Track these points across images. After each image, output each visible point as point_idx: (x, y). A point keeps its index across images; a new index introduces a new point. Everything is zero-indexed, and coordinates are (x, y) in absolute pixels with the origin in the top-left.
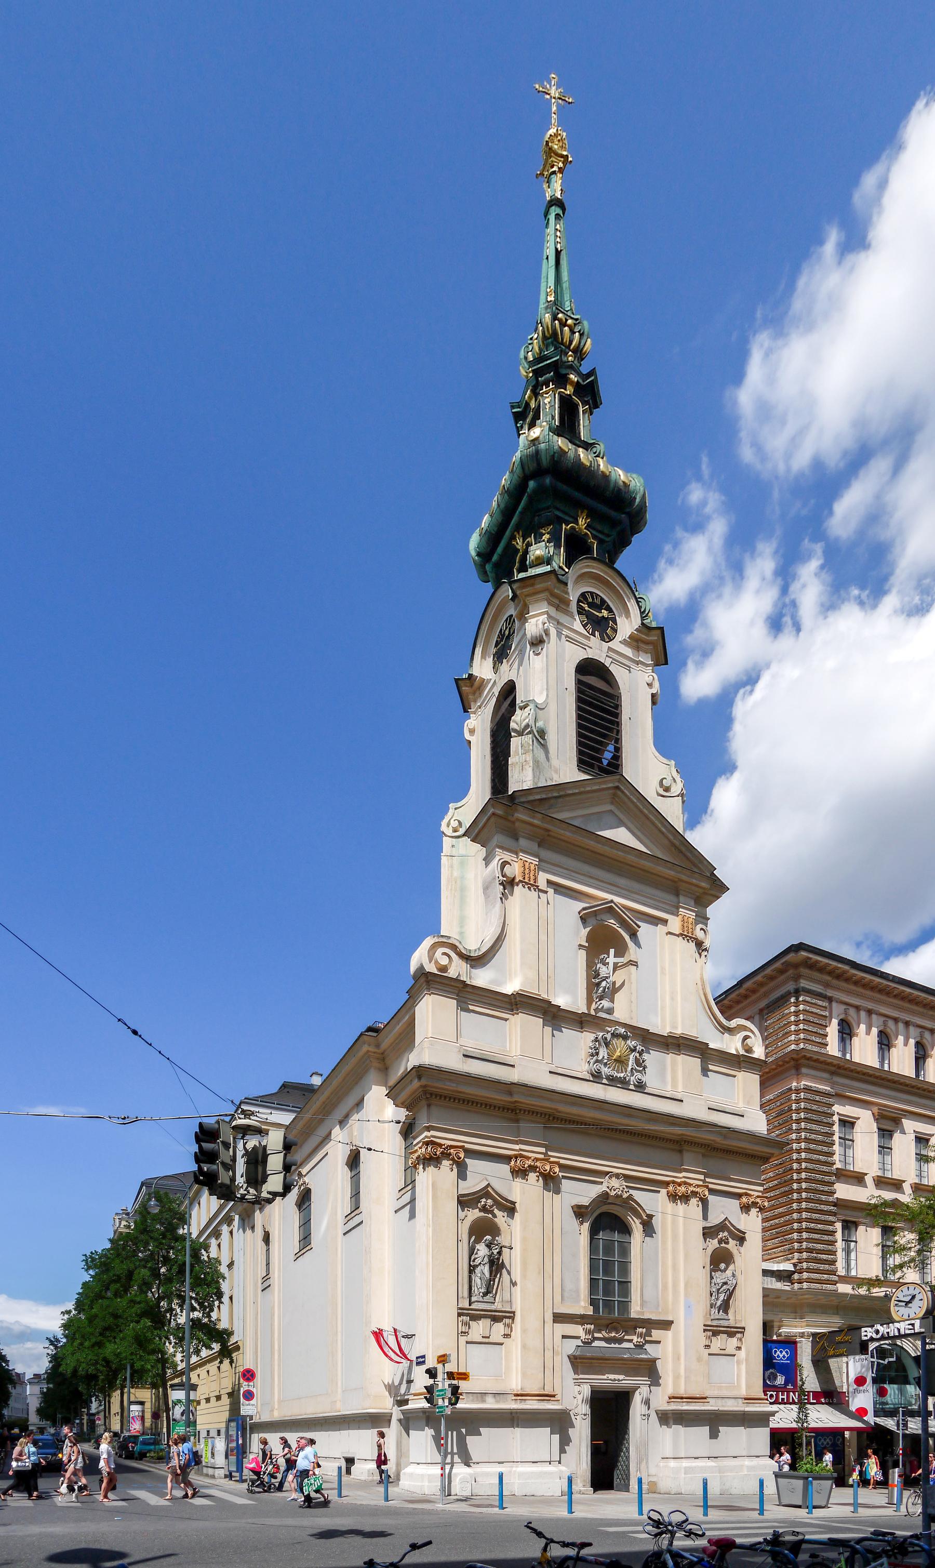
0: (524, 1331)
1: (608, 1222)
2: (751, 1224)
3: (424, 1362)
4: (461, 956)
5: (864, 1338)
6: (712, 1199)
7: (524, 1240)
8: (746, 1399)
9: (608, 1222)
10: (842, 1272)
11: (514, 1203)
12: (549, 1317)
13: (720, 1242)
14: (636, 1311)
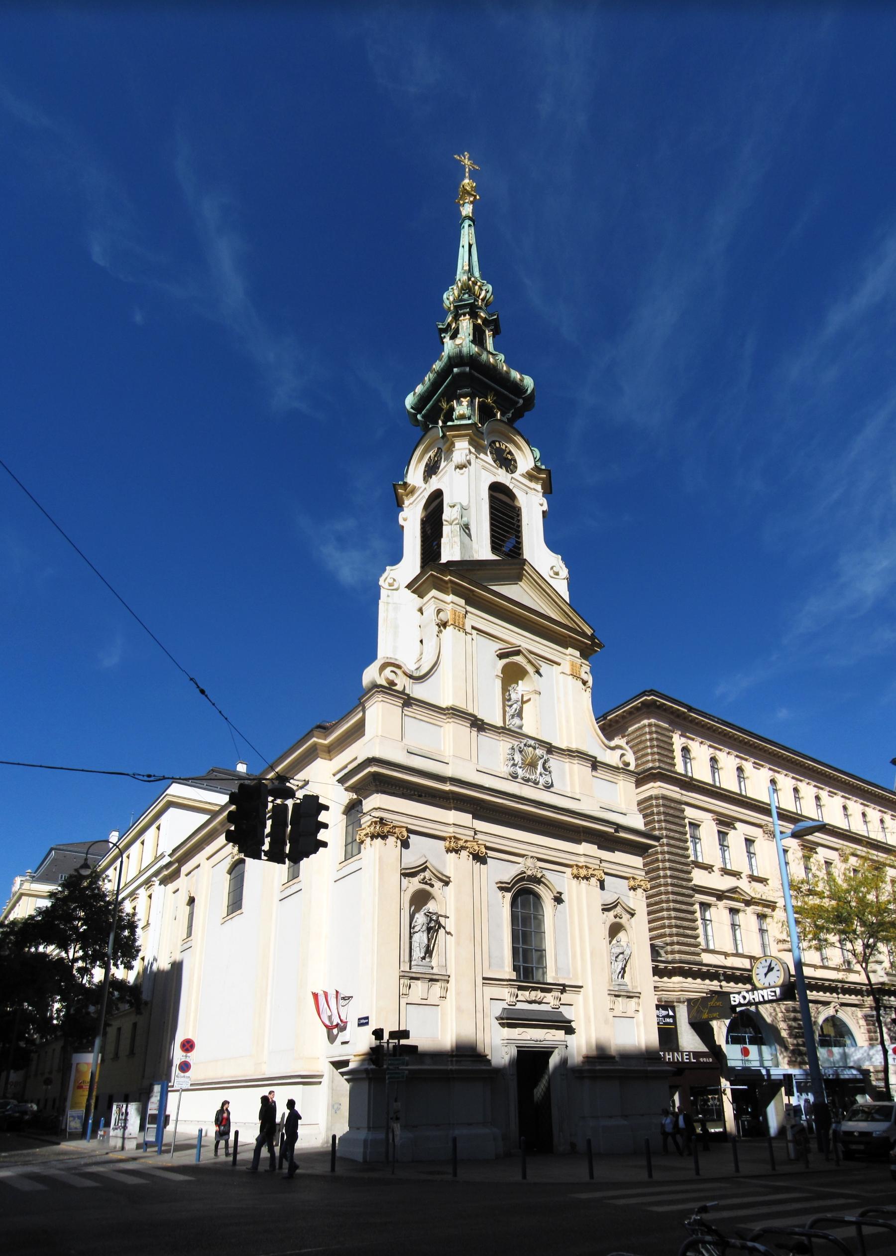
0: (458, 994)
1: (525, 897)
2: (638, 901)
4: (405, 673)
5: (733, 1003)
6: (608, 880)
8: (648, 1059)
9: (525, 897)
10: (703, 946)
12: (480, 981)
13: (615, 917)
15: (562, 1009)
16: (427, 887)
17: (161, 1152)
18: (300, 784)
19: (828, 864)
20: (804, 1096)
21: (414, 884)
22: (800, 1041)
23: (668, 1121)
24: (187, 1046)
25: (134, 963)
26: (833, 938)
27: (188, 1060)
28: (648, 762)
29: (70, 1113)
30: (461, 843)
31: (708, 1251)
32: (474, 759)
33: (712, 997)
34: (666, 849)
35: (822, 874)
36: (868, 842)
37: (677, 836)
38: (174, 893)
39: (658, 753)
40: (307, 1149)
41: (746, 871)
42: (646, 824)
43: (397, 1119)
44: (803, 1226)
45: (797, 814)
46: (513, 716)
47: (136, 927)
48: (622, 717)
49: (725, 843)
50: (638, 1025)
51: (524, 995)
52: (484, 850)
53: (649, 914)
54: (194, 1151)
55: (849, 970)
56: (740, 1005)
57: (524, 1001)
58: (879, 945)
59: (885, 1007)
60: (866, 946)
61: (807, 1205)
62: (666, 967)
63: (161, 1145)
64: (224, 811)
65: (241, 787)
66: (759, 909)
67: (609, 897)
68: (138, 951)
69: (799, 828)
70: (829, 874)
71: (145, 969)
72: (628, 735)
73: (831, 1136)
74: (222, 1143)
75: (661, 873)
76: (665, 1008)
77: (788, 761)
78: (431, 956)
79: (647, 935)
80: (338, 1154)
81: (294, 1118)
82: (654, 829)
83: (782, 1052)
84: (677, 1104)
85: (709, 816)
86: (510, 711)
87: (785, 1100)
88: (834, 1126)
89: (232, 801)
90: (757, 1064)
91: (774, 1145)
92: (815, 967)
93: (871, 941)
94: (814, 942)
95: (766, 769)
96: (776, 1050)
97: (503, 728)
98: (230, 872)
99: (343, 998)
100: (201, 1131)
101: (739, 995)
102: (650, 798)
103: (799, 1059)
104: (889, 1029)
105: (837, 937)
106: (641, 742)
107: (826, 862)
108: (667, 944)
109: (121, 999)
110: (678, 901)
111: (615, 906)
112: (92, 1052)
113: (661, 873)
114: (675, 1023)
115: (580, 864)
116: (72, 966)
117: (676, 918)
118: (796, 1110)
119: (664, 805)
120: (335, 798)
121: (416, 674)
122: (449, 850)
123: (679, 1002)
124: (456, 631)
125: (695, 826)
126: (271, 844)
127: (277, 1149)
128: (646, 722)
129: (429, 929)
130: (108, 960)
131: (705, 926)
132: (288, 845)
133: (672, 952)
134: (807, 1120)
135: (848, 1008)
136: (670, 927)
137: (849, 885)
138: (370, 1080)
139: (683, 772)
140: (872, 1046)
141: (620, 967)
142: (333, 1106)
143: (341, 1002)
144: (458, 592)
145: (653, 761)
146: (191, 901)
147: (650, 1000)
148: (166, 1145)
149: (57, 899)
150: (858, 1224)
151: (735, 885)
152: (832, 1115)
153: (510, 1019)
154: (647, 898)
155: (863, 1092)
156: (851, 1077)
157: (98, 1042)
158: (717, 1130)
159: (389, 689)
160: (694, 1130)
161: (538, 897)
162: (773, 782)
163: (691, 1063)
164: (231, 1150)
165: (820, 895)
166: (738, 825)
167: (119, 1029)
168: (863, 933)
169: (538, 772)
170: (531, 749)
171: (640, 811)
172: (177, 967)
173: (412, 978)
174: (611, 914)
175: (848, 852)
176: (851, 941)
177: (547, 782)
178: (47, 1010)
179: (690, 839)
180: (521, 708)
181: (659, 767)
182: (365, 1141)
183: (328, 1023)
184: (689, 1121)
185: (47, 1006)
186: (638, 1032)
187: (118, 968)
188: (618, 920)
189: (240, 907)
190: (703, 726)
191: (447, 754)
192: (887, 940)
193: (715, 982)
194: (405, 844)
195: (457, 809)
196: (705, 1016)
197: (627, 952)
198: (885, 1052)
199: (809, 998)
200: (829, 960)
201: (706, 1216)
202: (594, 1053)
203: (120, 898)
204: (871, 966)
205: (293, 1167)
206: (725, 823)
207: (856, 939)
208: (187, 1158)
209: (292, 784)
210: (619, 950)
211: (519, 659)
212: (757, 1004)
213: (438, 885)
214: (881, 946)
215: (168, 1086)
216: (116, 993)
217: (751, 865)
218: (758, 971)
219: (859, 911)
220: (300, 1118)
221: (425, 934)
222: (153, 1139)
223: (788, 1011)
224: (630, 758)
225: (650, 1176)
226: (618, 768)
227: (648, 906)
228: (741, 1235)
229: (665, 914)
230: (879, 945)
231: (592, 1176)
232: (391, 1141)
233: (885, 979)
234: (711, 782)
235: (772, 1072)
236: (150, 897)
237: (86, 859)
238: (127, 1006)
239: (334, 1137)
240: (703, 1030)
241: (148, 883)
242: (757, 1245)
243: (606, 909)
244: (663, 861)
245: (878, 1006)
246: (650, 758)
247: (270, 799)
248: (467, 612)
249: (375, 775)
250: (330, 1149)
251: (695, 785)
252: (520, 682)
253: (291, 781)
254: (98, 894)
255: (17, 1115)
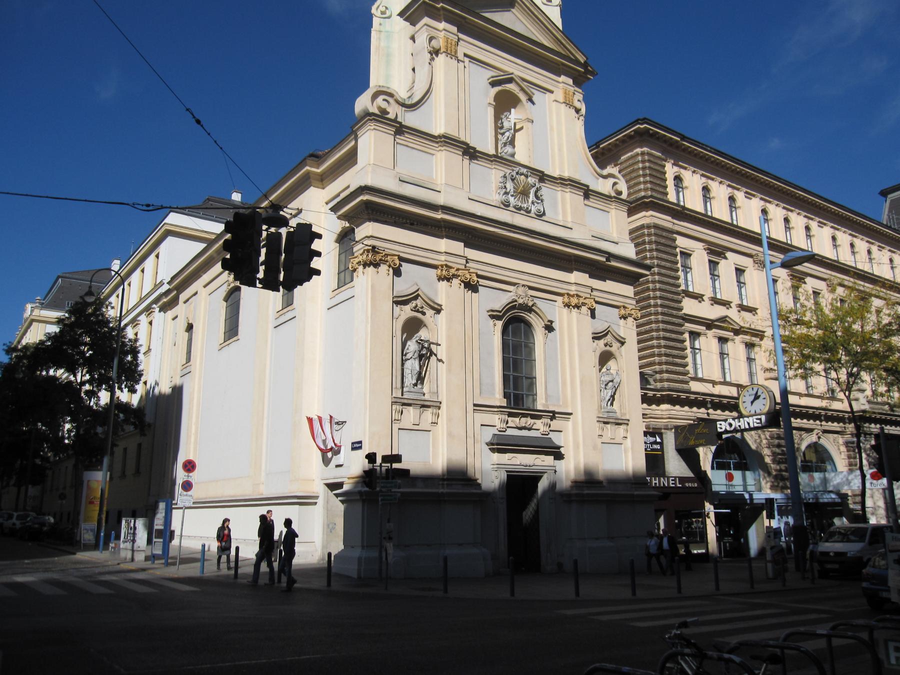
0: (449, 420)
1: (516, 325)
2: (628, 330)
3: (360, 448)
4: (397, 102)
5: (719, 430)
6: (599, 308)
7: (449, 338)
8: (635, 484)
9: (516, 325)
11: (441, 306)
12: (470, 408)
13: (606, 345)
14: (540, 405)
15: (552, 436)
16: (419, 315)
17: (167, 564)
18: (294, 212)
19: (816, 293)
20: (784, 519)
21: (406, 312)
22: (783, 466)
23: (652, 543)
24: (189, 466)
25: (137, 387)
26: (818, 367)
27: (190, 479)
28: (640, 190)
29: (83, 526)
30: (453, 271)
31: (686, 662)
32: (466, 188)
33: (699, 424)
34: (657, 278)
35: (810, 304)
36: (855, 273)
37: (668, 265)
38: (173, 319)
39: (651, 182)
40: (304, 565)
41: (736, 301)
42: (637, 253)
43: (390, 538)
44: (777, 639)
45: (787, 244)
46: (505, 144)
47: (138, 352)
48: (615, 145)
49: (716, 273)
50: (626, 451)
51: (514, 421)
52: (475, 279)
53: (639, 342)
54: (198, 564)
55: (833, 398)
56: (726, 432)
57: (515, 426)
58: (863, 373)
59: (866, 434)
60: (850, 375)
61: (782, 620)
62: (655, 395)
63: (168, 558)
64: (220, 240)
65: (236, 215)
66: (747, 338)
67: (600, 326)
68: (141, 375)
69: (788, 259)
70: (817, 303)
71: (148, 393)
72: (621, 164)
73: (808, 557)
74: (224, 558)
75: (652, 302)
76: (653, 434)
77: (779, 191)
78: (422, 383)
79: (636, 363)
80: (333, 570)
81: (291, 536)
82: (645, 258)
83: (765, 478)
84: (662, 526)
85: (700, 245)
86: (503, 139)
87: (766, 523)
88: (811, 547)
89: (227, 230)
90: (741, 488)
91: (753, 565)
92: (800, 395)
93: (855, 369)
94: (800, 371)
95: (758, 199)
96: (759, 475)
97: (496, 156)
98: (226, 299)
99: (337, 423)
100: (204, 546)
101: (725, 423)
102: (642, 227)
103: (781, 484)
104: (868, 455)
105: (822, 366)
106: (633, 171)
107: (814, 292)
108: (656, 372)
109: (126, 421)
110: (668, 330)
111: (606, 335)
112: (101, 470)
113: (652, 302)
114: (662, 449)
115: (572, 293)
116: (80, 389)
117: (666, 347)
118: (776, 532)
119: (655, 235)
120: (327, 225)
121: (408, 102)
122: (440, 279)
123: (667, 429)
124: (448, 58)
125: (686, 255)
126: (265, 271)
127: (276, 565)
128: (639, 150)
129: (421, 357)
130: (113, 384)
131: (694, 355)
132: (282, 273)
133: (661, 381)
134: (786, 542)
135: (831, 435)
136: (660, 355)
137: (835, 315)
138: (364, 501)
139: (675, 201)
140: (851, 471)
141: (609, 394)
142: (328, 525)
143: (335, 427)
144: (450, 19)
145: (646, 190)
146: (190, 328)
147: (638, 426)
148: (172, 558)
149: (65, 325)
150: (829, 637)
151: (724, 314)
152: (810, 536)
153: (500, 445)
154: (637, 327)
155: (840, 515)
156: (830, 500)
157: (106, 461)
158: (700, 551)
159: (381, 117)
160: (678, 551)
161: (528, 325)
162: (764, 212)
163: (676, 487)
164: (232, 565)
165: (808, 325)
166: (729, 254)
167: (125, 449)
168: (847, 362)
169: (530, 201)
170: (523, 177)
171: (632, 240)
172: (178, 391)
173: (404, 404)
174: (602, 342)
175: (835, 282)
176: (836, 370)
177: (539, 211)
178: (59, 430)
179: (681, 269)
180: (514, 136)
181: (651, 196)
182: (360, 559)
183: (322, 447)
184: (673, 543)
185: (59, 427)
186: (626, 458)
187: (122, 391)
188: (608, 348)
189: (236, 334)
190: (696, 155)
191: (439, 182)
192: (869, 369)
193: (703, 410)
194: (397, 272)
195: (448, 237)
196: (692, 443)
197: (617, 380)
198: (863, 477)
199: (794, 425)
200: (813, 388)
201: (685, 631)
202: (582, 478)
203: (123, 324)
204: (854, 394)
205: (291, 581)
206: (716, 253)
207: (840, 368)
208: (192, 570)
209: (285, 213)
210: (608, 378)
211: (511, 87)
212: (742, 431)
213: (430, 313)
214: (865, 376)
215: (172, 504)
216: (121, 415)
217: (741, 294)
218: (744, 399)
219: (845, 341)
220: (297, 536)
221: (417, 362)
222: (160, 552)
223: (772, 437)
224: (623, 186)
225: (634, 594)
226: (610, 197)
227: (638, 334)
228: (718, 648)
229: (655, 342)
230: (863, 373)
231: (577, 594)
232: (384, 559)
233: (867, 407)
234: (703, 211)
235: (755, 496)
236: (151, 323)
237: (90, 287)
238: (132, 428)
239: (330, 555)
240: (689, 456)
241: (148, 310)
242: (733, 657)
243: (597, 337)
244: (654, 290)
245: (858, 433)
246: (642, 186)
247: (264, 227)
248: (459, 39)
249: (367, 204)
250: (326, 565)
251: (687, 214)
252: (513, 110)
253: (285, 209)
254: (102, 321)
255: (36, 526)
